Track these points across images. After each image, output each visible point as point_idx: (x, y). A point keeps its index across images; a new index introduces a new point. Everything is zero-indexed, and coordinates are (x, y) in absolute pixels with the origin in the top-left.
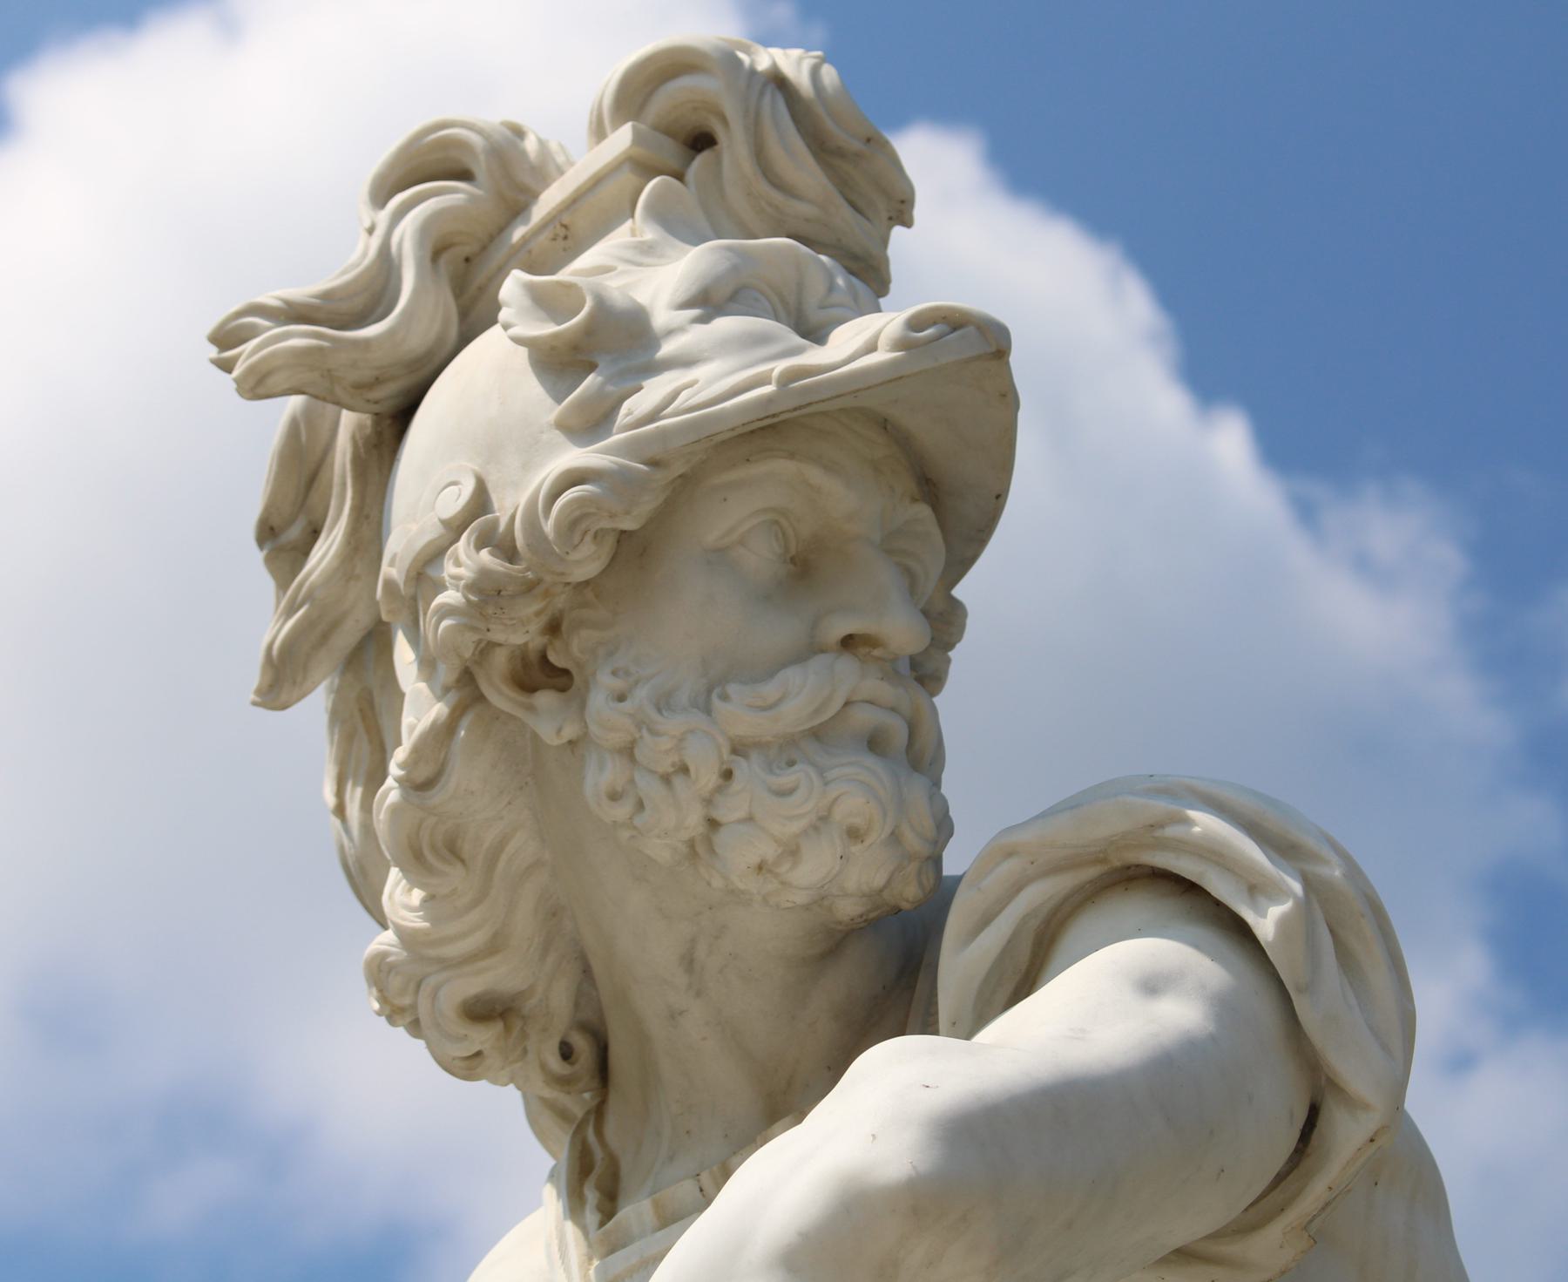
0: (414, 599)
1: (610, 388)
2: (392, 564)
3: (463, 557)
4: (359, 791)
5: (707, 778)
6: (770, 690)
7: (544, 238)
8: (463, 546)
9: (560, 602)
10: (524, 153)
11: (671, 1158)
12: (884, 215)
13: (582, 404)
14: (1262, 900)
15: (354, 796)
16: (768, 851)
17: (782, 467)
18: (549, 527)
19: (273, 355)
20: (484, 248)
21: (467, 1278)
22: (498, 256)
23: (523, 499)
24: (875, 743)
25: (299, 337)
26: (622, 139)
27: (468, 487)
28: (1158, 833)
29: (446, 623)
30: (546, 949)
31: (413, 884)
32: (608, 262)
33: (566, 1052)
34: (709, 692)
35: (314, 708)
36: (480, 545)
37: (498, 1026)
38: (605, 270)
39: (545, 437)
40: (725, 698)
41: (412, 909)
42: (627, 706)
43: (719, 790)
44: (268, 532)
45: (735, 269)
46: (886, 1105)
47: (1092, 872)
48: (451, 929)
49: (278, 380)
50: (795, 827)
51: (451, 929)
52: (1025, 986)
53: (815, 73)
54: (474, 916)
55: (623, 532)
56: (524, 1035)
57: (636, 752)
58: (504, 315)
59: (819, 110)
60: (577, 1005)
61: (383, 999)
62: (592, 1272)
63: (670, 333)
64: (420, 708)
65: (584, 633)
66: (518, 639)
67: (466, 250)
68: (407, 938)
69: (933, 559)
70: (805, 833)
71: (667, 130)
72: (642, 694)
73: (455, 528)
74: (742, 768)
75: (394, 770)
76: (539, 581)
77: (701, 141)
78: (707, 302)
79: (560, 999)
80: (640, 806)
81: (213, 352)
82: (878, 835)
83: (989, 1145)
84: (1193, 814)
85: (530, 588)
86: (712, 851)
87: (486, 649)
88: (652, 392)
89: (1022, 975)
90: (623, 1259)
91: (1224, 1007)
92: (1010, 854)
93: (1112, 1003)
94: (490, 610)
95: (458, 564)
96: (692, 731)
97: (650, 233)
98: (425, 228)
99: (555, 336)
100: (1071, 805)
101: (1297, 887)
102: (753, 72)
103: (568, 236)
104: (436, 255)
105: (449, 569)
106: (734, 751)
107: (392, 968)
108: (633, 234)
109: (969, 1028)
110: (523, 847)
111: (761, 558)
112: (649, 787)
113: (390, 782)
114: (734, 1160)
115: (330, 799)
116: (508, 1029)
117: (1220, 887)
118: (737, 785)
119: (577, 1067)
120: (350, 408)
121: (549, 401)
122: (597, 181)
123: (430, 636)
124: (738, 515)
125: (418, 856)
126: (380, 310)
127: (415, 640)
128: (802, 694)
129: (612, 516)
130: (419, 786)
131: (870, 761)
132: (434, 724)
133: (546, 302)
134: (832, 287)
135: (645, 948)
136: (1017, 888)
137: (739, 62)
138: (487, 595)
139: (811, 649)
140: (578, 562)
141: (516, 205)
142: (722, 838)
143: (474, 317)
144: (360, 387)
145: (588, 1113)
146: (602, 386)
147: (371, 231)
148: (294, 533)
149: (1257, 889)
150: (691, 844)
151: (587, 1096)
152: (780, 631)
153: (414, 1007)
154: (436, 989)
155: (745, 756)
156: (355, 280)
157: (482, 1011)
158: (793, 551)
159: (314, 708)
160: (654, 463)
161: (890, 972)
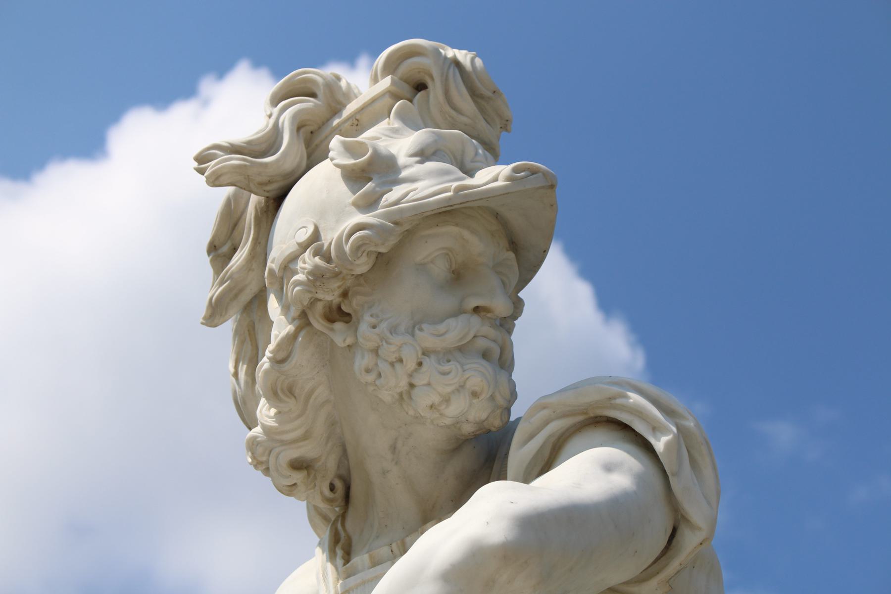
0: (282, 278)
1: (378, 189)
2: (273, 262)
3: (307, 259)
4: (245, 366)
5: (411, 365)
6: (442, 328)
7: (347, 125)
8: (307, 255)
9: (349, 283)
10: (340, 87)
11: (378, 537)
12: (499, 127)
13: (365, 195)
14: (658, 434)
15: (243, 369)
16: (436, 399)
17: (452, 229)
18: (347, 248)
19: (223, 167)
20: (320, 128)
21: (275, 591)
22: (326, 131)
23: (336, 235)
24: (485, 355)
25: (236, 160)
26: (386, 82)
27: (311, 229)
28: (613, 402)
29: (297, 288)
30: (328, 439)
31: (271, 406)
32: (378, 135)
33: (332, 488)
34: (414, 327)
35: (228, 327)
36: (315, 255)
37: (305, 472)
38: (377, 138)
39: (347, 209)
40: (421, 330)
41: (270, 417)
42: (376, 330)
43: (416, 370)
44: (213, 248)
45: (435, 141)
46: (490, 511)
47: (580, 418)
48: (288, 427)
49: (225, 179)
50: (449, 389)
51: (288, 427)
52: (547, 467)
53: (472, 60)
54: (297, 423)
55: (380, 253)
56: (315, 478)
57: (380, 352)
58: (331, 154)
59: (474, 77)
60: (338, 467)
61: (254, 457)
62: (339, 586)
63: (406, 167)
64: (280, 325)
65: (359, 297)
66: (329, 298)
67: (311, 128)
68: (267, 430)
69: (514, 279)
70: (453, 392)
71: (406, 81)
72: (384, 326)
73: (304, 247)
74: (427, 362)
75: (268, 354)
76: (340, 273)
77: (420, 87)
78: (423, 155)
79: (331, 464)
80: (380, 375)
81: (196, 164)
82: (485, 396)
83: (541, 532)
84: (630, 394)
85: (336, 275)
86: (410, 398)
87: (314, 301)
88: (396, 192)
89: (546, 462)
90: (353, 581)
91: (640, 479)
92: (544, 407)
93: (590, 474)
94: (318, 284)
95: (304, 262)
96: (405, 344)
97: (397, 124)
98: (294, 117)
99: (354, 164)
100: (574, 387)
101: (674, 429)
102: (446, 58)
103: (358, 124)
104: (299, 128)
105: (300, 264)
106: (424, 354)
107: (259, 443)
108: (389, 124)
109: (527, 477)
110: (322, 393)
111: (440, 269)
112: (384, 367)
113: (265, 359)
114: (408, 540)
115: (232, 370)
116: (309, 474)
117: (640, 427)
118: (424, 368)
119: (336, 495)
120: (256, 194)
121: (350, 193)
122: (374, 101)
123: (289, 295)
124: (431, 249)
125: (275, 393)
126: (272, 151)
127: (280, 297)
128: (456, 330)
129: (376, 245)
130: (278, 361)
131: (484, 362)
132: (288, 334)
133: (350, 150)
134: (477, 153)
135: (374, 439)
136: (547, 423)
137: (440, 53)
138: (317, 277)
139: (459, 312)
140: (359, 265)
141: (335, 109)
142: (416, 392)
143: (314, 154)
144: (261, 184)
145: (338, 517)
146: (374, 188)
147: (270, 116)
148: (225, 249)
149: (656, 429)
150: (401, 394)
151: (337, 509)
152: (447, 303)
153: (267, 462)
154: (278, 454)
155: (428, 356)
156: (263, 137)
157: (298, 465)
158: (453, 268)
159: (228, 327)
160: (396, 223)
161: (484, 456)
